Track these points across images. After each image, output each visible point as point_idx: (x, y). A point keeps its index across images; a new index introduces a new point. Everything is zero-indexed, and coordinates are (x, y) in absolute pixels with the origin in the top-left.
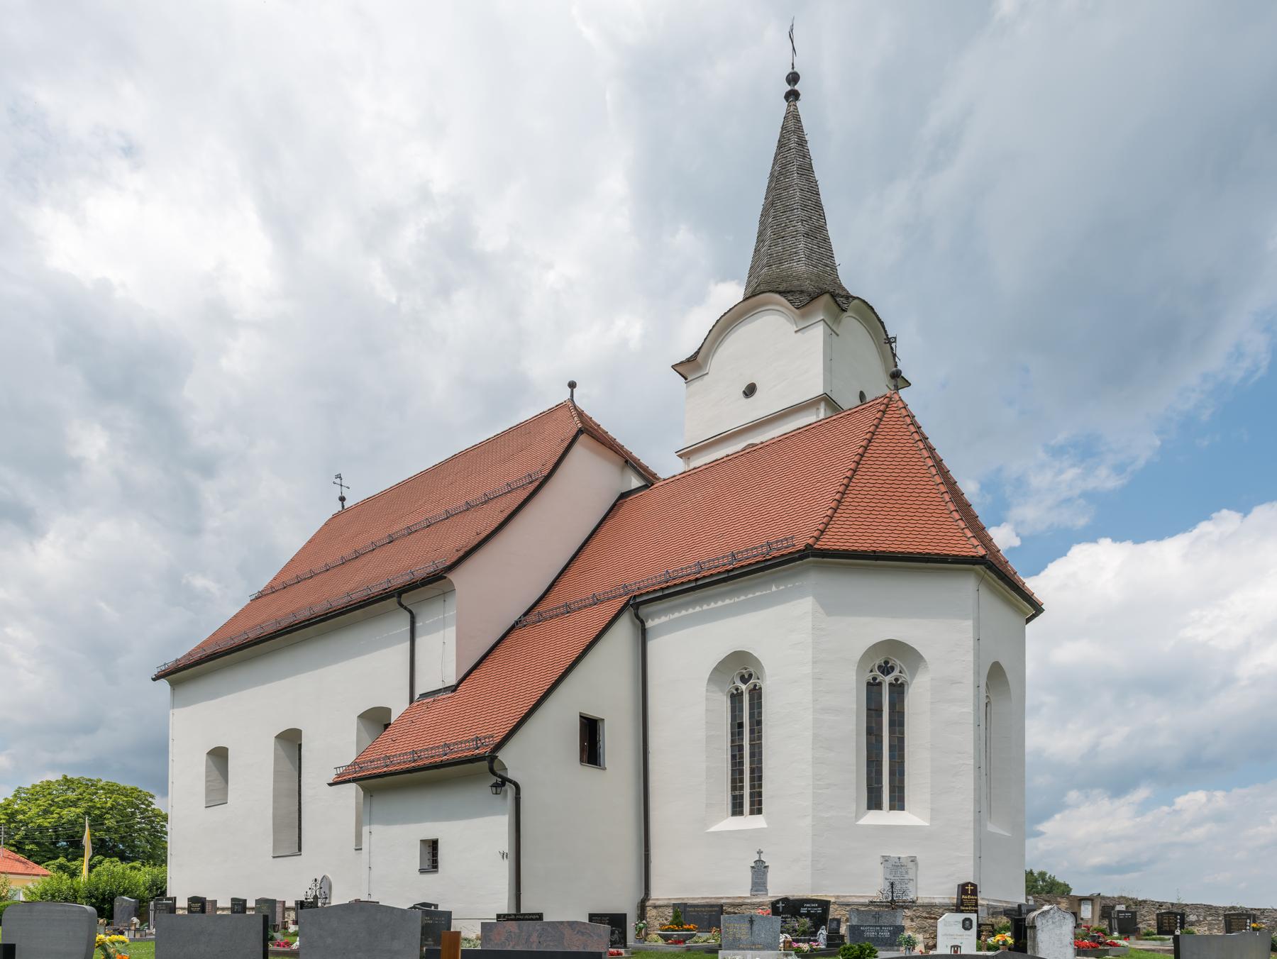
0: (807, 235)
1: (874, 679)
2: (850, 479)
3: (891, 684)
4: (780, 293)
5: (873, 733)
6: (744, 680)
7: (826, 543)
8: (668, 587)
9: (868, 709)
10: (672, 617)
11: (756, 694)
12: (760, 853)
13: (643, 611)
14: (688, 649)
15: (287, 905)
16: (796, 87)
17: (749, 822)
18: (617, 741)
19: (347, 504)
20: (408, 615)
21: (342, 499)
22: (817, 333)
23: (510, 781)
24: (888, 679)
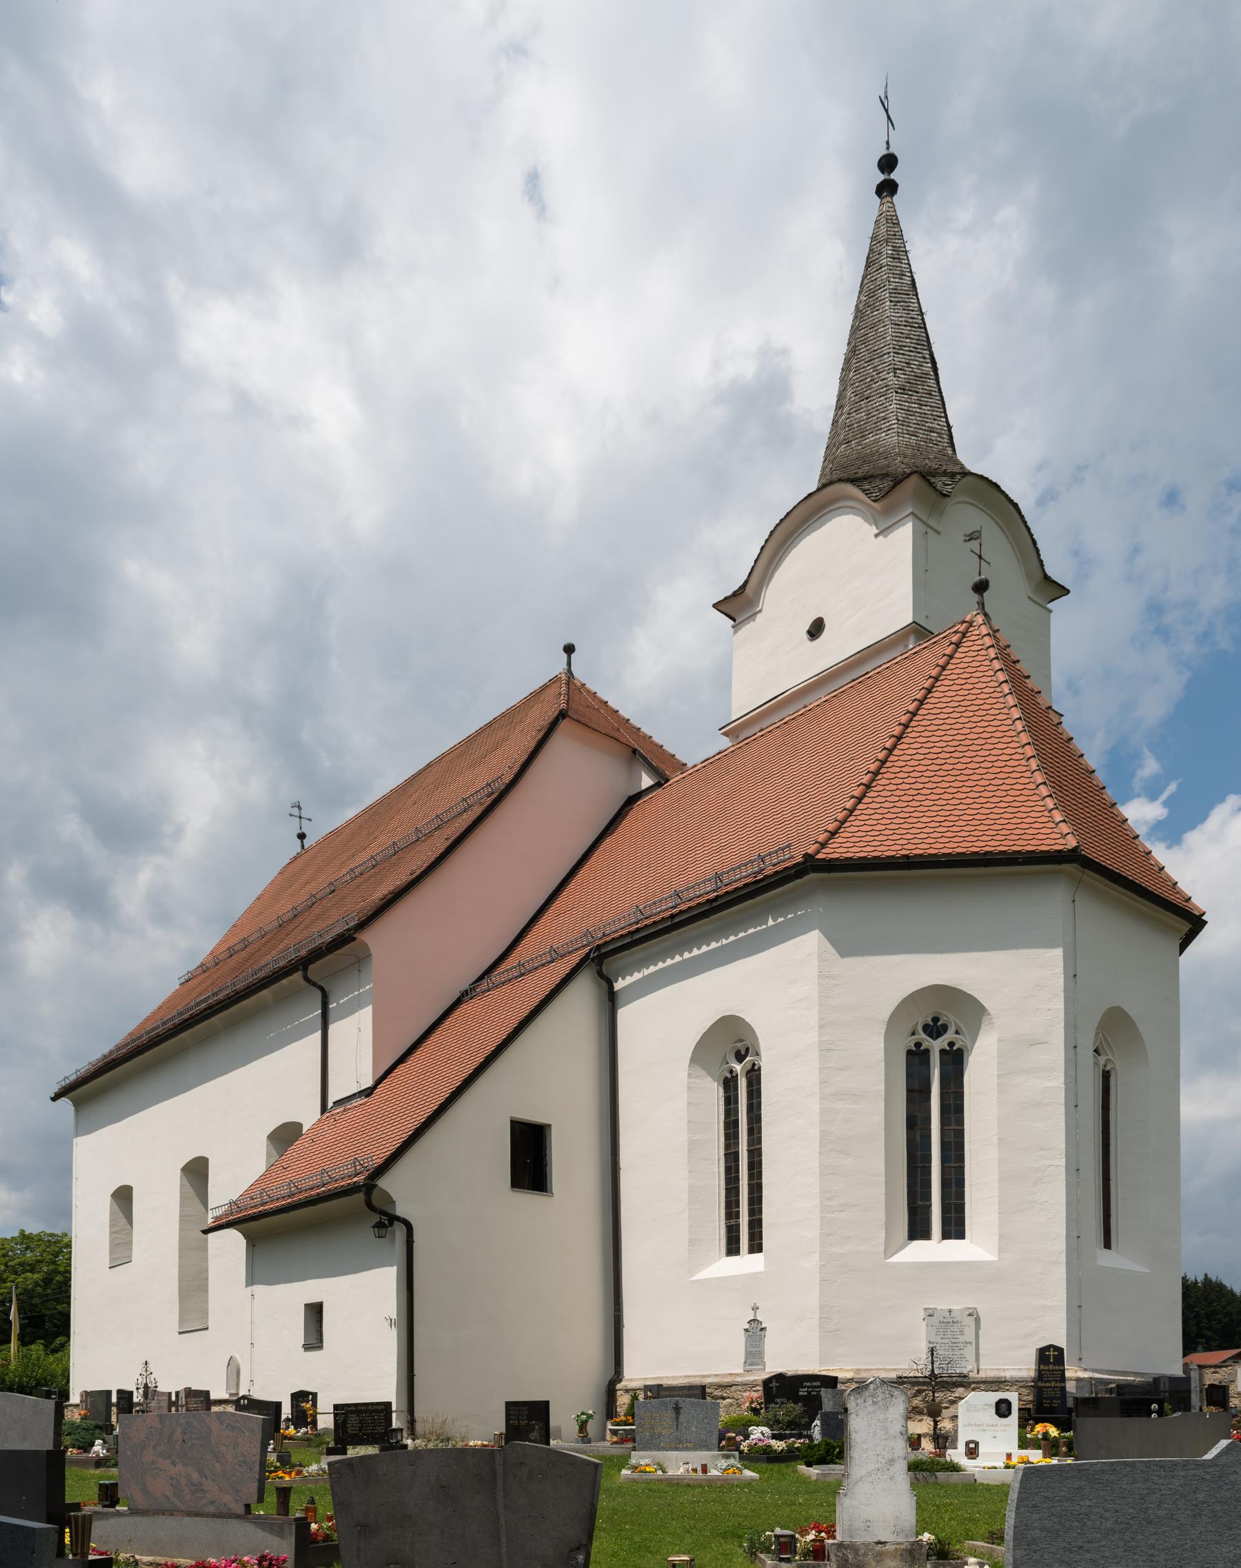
0: (902, 390)
1: (918, 1045)
2: (890, 751)
3: (942, 1052)
4: (853, 481)
5: (916, 1124)
6: (740, 1057)
7: (838, 850)
8: (638, 930)
9: (909, 1091)
10: (646, 972)
11: (754, 1076)
12: (755, 1309)
13: (609, 966)
14: (665, 1018)
15: (213, 1397)
16: (893, 176)
17: (746, 1263)
18: (572, 1158)
19: (307, 843)
20: (318, 994)
21: (302, 836)
22: (905, 534)
23: (399, 1219)
24: (936, 1046)
